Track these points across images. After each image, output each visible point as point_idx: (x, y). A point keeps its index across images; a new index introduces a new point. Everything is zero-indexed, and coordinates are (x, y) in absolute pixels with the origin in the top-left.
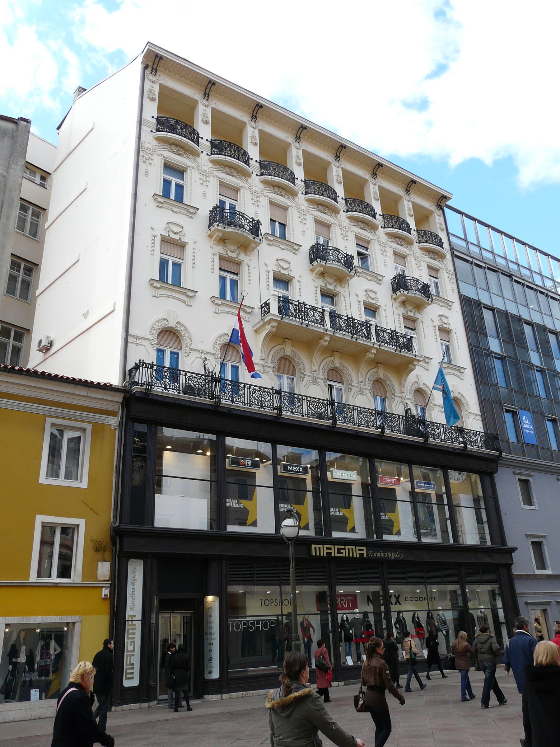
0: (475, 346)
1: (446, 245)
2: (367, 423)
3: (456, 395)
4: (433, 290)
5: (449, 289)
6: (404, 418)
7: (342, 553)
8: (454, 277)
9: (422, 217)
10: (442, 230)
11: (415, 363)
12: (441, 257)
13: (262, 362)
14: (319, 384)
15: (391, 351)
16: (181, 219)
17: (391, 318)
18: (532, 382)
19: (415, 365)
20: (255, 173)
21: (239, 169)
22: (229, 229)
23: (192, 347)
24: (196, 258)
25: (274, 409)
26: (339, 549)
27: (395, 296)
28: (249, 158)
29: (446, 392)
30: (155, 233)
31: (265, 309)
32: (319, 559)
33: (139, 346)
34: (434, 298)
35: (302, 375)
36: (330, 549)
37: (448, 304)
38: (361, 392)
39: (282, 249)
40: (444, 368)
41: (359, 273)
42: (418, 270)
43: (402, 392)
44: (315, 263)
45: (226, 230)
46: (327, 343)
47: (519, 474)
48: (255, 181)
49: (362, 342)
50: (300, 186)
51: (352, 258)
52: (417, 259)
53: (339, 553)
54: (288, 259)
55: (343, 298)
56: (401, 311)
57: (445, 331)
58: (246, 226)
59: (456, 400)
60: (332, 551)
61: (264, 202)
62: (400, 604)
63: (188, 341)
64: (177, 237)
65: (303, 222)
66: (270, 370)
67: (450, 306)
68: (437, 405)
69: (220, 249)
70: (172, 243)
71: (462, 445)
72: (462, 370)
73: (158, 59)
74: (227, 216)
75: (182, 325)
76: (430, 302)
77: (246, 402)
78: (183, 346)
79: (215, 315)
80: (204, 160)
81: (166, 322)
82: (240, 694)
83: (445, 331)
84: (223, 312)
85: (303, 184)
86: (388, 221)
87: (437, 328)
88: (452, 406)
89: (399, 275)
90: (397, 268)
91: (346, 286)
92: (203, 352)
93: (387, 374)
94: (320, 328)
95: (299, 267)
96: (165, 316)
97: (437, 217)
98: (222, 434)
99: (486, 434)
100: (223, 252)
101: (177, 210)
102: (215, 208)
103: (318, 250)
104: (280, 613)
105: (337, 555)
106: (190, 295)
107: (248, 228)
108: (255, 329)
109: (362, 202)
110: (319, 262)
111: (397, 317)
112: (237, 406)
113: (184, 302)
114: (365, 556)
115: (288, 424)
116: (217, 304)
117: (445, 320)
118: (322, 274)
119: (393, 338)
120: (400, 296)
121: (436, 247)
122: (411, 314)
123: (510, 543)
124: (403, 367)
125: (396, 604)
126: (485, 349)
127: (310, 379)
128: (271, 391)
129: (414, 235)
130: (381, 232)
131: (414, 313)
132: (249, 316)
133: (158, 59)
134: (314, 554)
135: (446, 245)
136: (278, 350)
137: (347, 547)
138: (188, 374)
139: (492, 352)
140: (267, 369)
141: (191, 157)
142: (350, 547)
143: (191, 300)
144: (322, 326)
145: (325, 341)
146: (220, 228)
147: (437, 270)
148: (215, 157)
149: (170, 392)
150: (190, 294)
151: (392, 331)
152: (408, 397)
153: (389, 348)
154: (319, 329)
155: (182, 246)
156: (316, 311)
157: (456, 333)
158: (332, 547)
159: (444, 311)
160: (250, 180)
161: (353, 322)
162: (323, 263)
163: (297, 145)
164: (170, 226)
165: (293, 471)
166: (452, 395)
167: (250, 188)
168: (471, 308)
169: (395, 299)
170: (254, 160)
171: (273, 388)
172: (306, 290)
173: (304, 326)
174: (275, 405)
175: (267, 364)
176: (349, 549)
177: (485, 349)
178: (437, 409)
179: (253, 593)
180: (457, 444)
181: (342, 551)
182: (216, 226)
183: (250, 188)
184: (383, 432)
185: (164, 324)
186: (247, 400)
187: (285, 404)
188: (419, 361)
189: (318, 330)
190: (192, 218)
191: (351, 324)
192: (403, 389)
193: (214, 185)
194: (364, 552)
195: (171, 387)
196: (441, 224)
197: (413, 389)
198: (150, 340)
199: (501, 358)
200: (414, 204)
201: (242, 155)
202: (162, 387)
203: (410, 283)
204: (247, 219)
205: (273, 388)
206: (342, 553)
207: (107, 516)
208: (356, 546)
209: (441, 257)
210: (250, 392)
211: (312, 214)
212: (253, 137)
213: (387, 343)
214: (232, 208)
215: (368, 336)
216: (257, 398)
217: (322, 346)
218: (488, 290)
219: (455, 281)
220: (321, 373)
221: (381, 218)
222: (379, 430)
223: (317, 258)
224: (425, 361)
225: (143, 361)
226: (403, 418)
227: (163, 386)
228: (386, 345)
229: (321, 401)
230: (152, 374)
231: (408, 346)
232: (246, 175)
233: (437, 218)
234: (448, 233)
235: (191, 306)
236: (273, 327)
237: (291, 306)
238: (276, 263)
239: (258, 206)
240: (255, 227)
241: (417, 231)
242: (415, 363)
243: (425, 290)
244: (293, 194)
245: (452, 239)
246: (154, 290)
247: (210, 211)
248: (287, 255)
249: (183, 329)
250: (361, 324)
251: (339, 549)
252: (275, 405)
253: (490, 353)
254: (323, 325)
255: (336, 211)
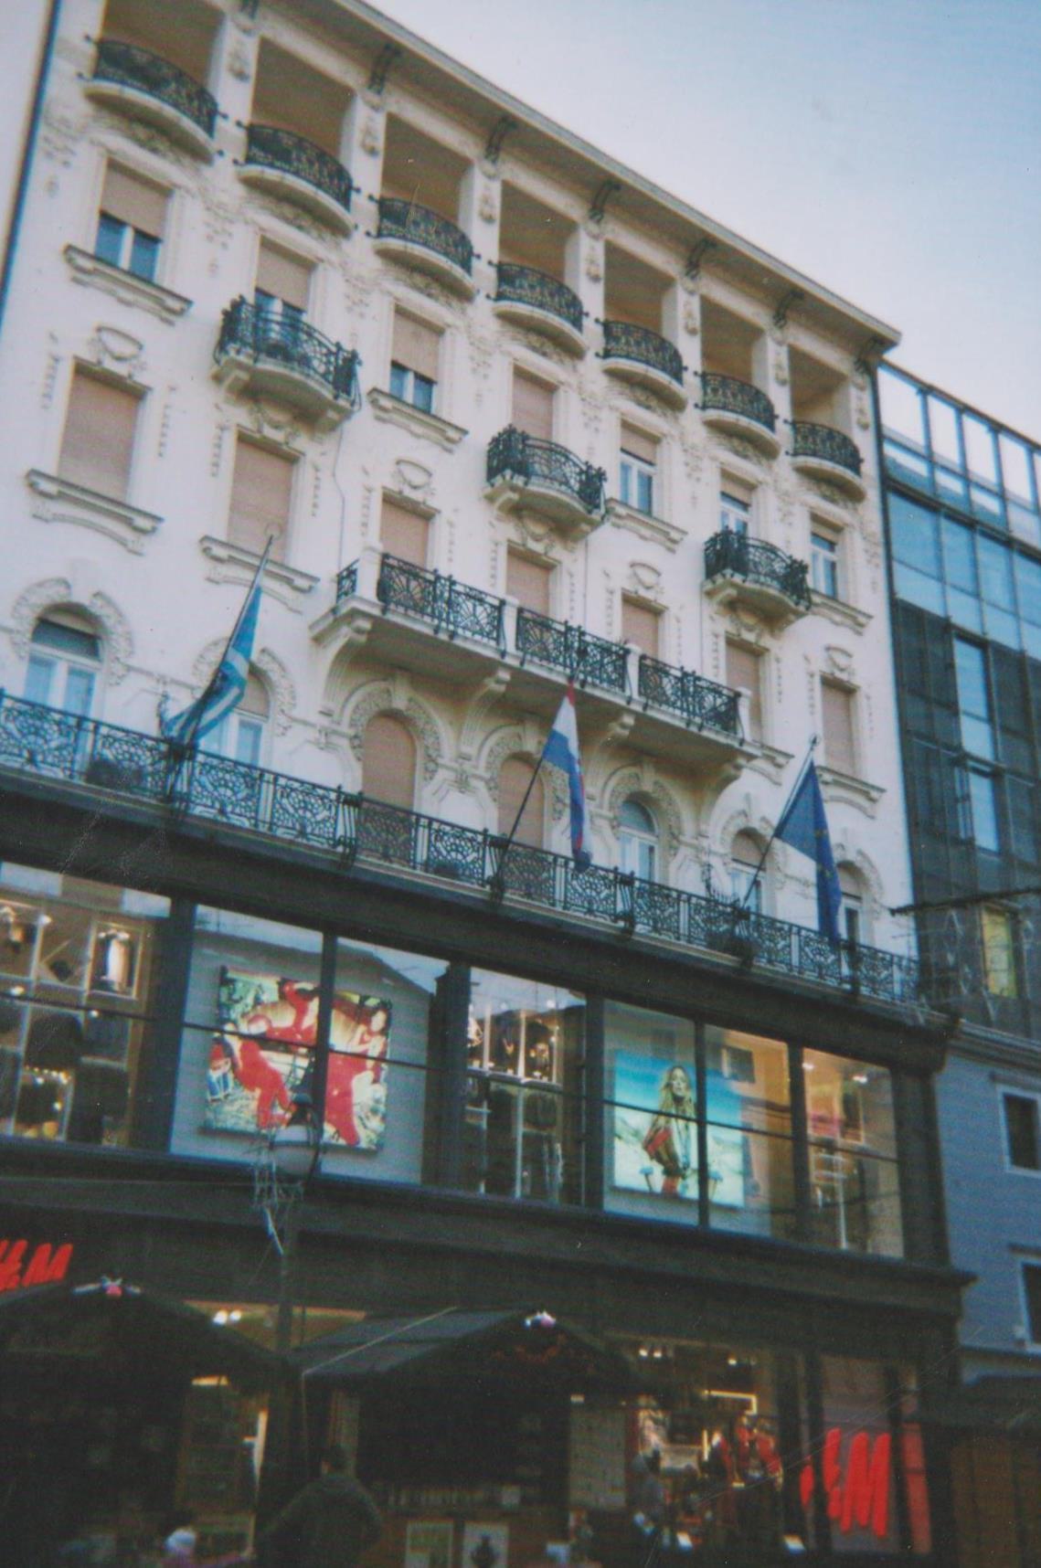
0: (920, 735)
1: (869, 468)
2: (590, 903)
3: (851, 856)
4: (816, 580)
5: (865, 587)
6: (572, 864)
8: (881, 551)
9: (814, 385)
10: (865, 427)
11: (741, 761)
12: (851, 494)
13: (325, 721)
14: (474, 791)
16: (139, 321)
17: (694, 641)
18: (956, 800)
19: (739, 768)
20: (362, 229)
22: (269, 365)
23: (133, 662)
25: (616, 918)
27: (709, 586)
28: (350, 187)
29: (819, 848)
31: (347, 583)
34: (816, 599)
35: (432, 766)
37: (856, 620)
38: (462, 783)
39: (836, 624)
40: (826, 783)
41: (619, 516)
42: (783, 521)
43: (701, 835)
44: (498, 480)
45: (260, 366)
46: (626, 733)
47: (1005, 1082)
48: (360, 251)
50: (483, 277)
51: (601, 475)
52: (785, 496)
54: (429, 464)
55: (566, 579)
56: (724, 625)
57: (839, 689)
58: (315, 363)
59: (848, 867)
61: (380, 309)
63: (123, 645)
64: (121, 369)
65: (696, 475)
66: (345, 743)
67: (862, 625)
68: (792, 878)
69: (241, 416)
71: (847, 987)
72: (780, 760)
74: (275, 334)
76: (802, 608)
78: (275, 705)
79: (208, 584)
80: (224, 177)
81: (62, 590)
83: (839, 689)
85: (599, 329)
86: (715, 391)
87: (817, 680)
88: (835, 880)
89: (726, 533)
90: (724, 515)
91: (580, 546)
92: (162, 680)
93: (421, 699)
94: (485, 646)
95: (456, 484)
97: (853, 391)
98: (461, 961)
99: (923, 965)
100: (515, 537)
102: (238, 305)
103: (508, 446)
106: (132, 521)
107: (322, 369)
108: (317, 631)
109: (561, 289)
111: (709, 641)
112: (312, 848)
113: (122, 542)
117: (842, 660)
118: (732, 606)
119: (685, 693)
120: (721, 588)
121: (840, 470)
122: (749, 637)
123: (961, 1255)
126: (949, 748)
127: (451, 776)
128: (480, 838)
129: (782, 435)
130: (784, 464)
131: (759, 636)
132: (301, 597)
135: (869, 468)
136: (368, 693)
138: (282, 781)
139: (968, 756)
140: (334, 739)
141: (328, 236)
143: (145, 540)
144: (493, 643)
145: (499, 682)
146: (242, 358)
147: (837, 529)
148: (254, 170)
150: (300, 582)
151: (685, 674)
152: (717, 848)
153: (671, 716)
154: (486, 649)
155: (135, 394)
156: (481, 601)
157: (678, 621)
159: (842, 637)
160: (470, 309)
161: (451, 590)
162: (738, 578)
163: (489, 167)
164: (106, 336)
166: (837, 856)
167: (344, 265)
168: (921, 641)
169: (710, 594)
170: (365, 192)
172: (470, 547)
174: (340, 832)
175: (335, 727)
177: (949, 748)
178: (792, 887)
180: (832, 982)
182: (232, 354)
183: (344, 265)
184: (629, 931)
185: (56, 595)
186: (795, 960)
187: (204, 787)
188: (751, 757)
190: (170, 323)
191: (575, 646)
192: (703, 827)
193: (501, 377)
196: (861, 411)
197: (733, 829)
198: (9, 631)
199: (995, 775)
200: (796, 356)
201: (456, 246)
202: (20, 755)
203: (754, 555)
204: (320, 344)
209: (851, 494)
210: (95, 742)
211: (509, 354)
212: (486, 201)
213: (481, 633)
214: (293, 313)
215: (621, 681)
216: (210, 788)
217: (491, 694)
218: (977, 595)
219: (881, 562)
220: (483, 763)
221: (697, 382)
222: (621, 924)
223: (725, 567)
224: (771, 760)
226: (566, 864)
227: (26, 754)
228: (477, 637)
229: (469, 835)
231: (727, 718)
232: (199, 155)
233: (856, 399)
234: (880, 437)
236: (359, 631)
237: (665, 681)
238: (95, 335)
239: (224, 245)
240: (345, 371)
241: (794, 424)
242: (741, 761)
243: (794, 576)
244: (573, 352)
245: (889, 450)
246: (212, 564)
247: (226, 313)
248: (425, 452)
249: (275, 667)
250: (605, 649)
252: (620, 907)
253: (961, 759)
254: (497, 640)
255: (573, 352)
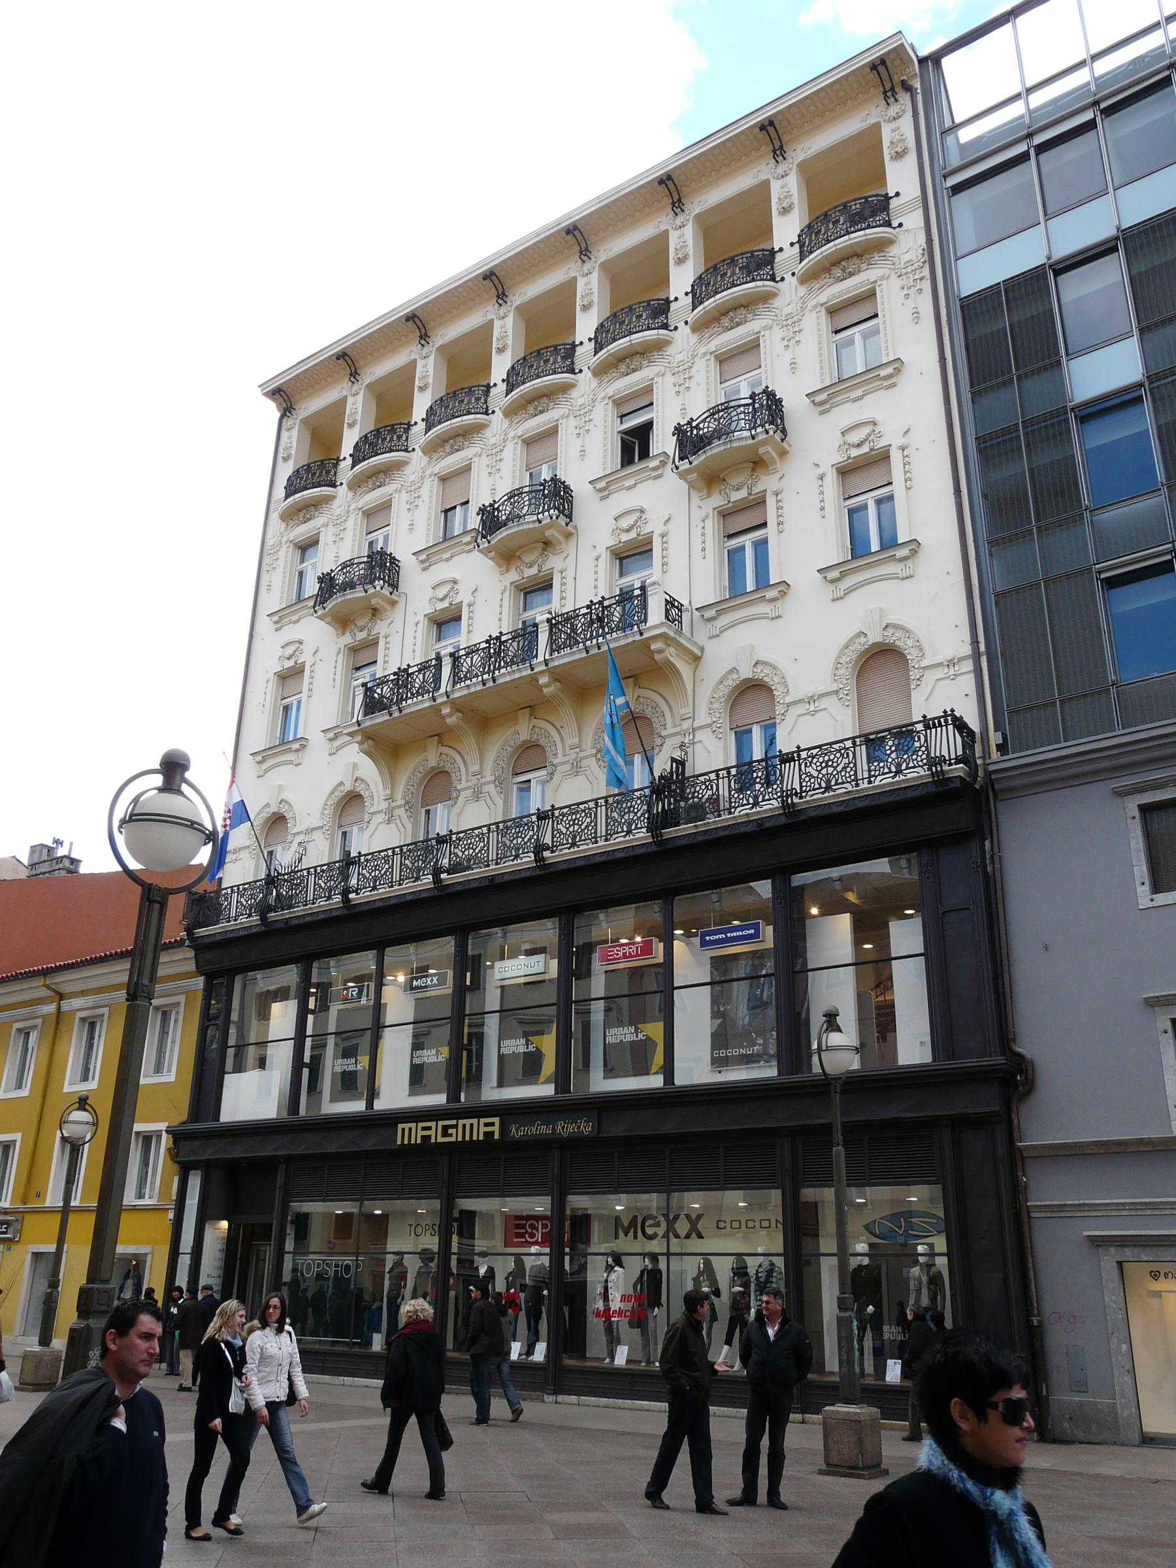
7: (451, 1135)
15: (577, 657)
21: (640, 349)
24: (785, 511)
26: (445, 1128)
30: (820, 471)
32: (409, 1150)
33: (819, 714)
36: (429, 1128)
49: (508, 679)
53: (445, 1134)
60: (432, 1133)
62: (700, 1236)
70: (290, 676)
73: (881, 69)
75: (896, 627)
77: (860, 777)
82: (604, 1401)
84: (848, 592)
96: (854, 630)
101: (631, 482)
104: (672, 1251)
105: (440, 1139)
110: (378, 588)
114: (497, 1136)
115: (379, 908)
116: (833, 581)
124: (647, 670)
125: (688, 1236)
133: (881, 69)
134: (399, 1142)
137: (461, 1122)
141: (876, 256)
142: (468, 1122)
149: (909, 776)
158: (433, 1124)
165: (421, 987)
171: (924, 717)
173: (595, 651)
176: (464, 1126)
179: (402, 1214)
181: (450, 1131)
185: (859, 646)
189: (419, 707)
194: (496, 1129)
195: (911, 765)
205: (924, 717)
206: (451, 1135)
207: (180, 1114)
208: (479, 1117)
225: (952, 710)
230: (730, 786)
235: (912, 576)
251: (445, 1128)
